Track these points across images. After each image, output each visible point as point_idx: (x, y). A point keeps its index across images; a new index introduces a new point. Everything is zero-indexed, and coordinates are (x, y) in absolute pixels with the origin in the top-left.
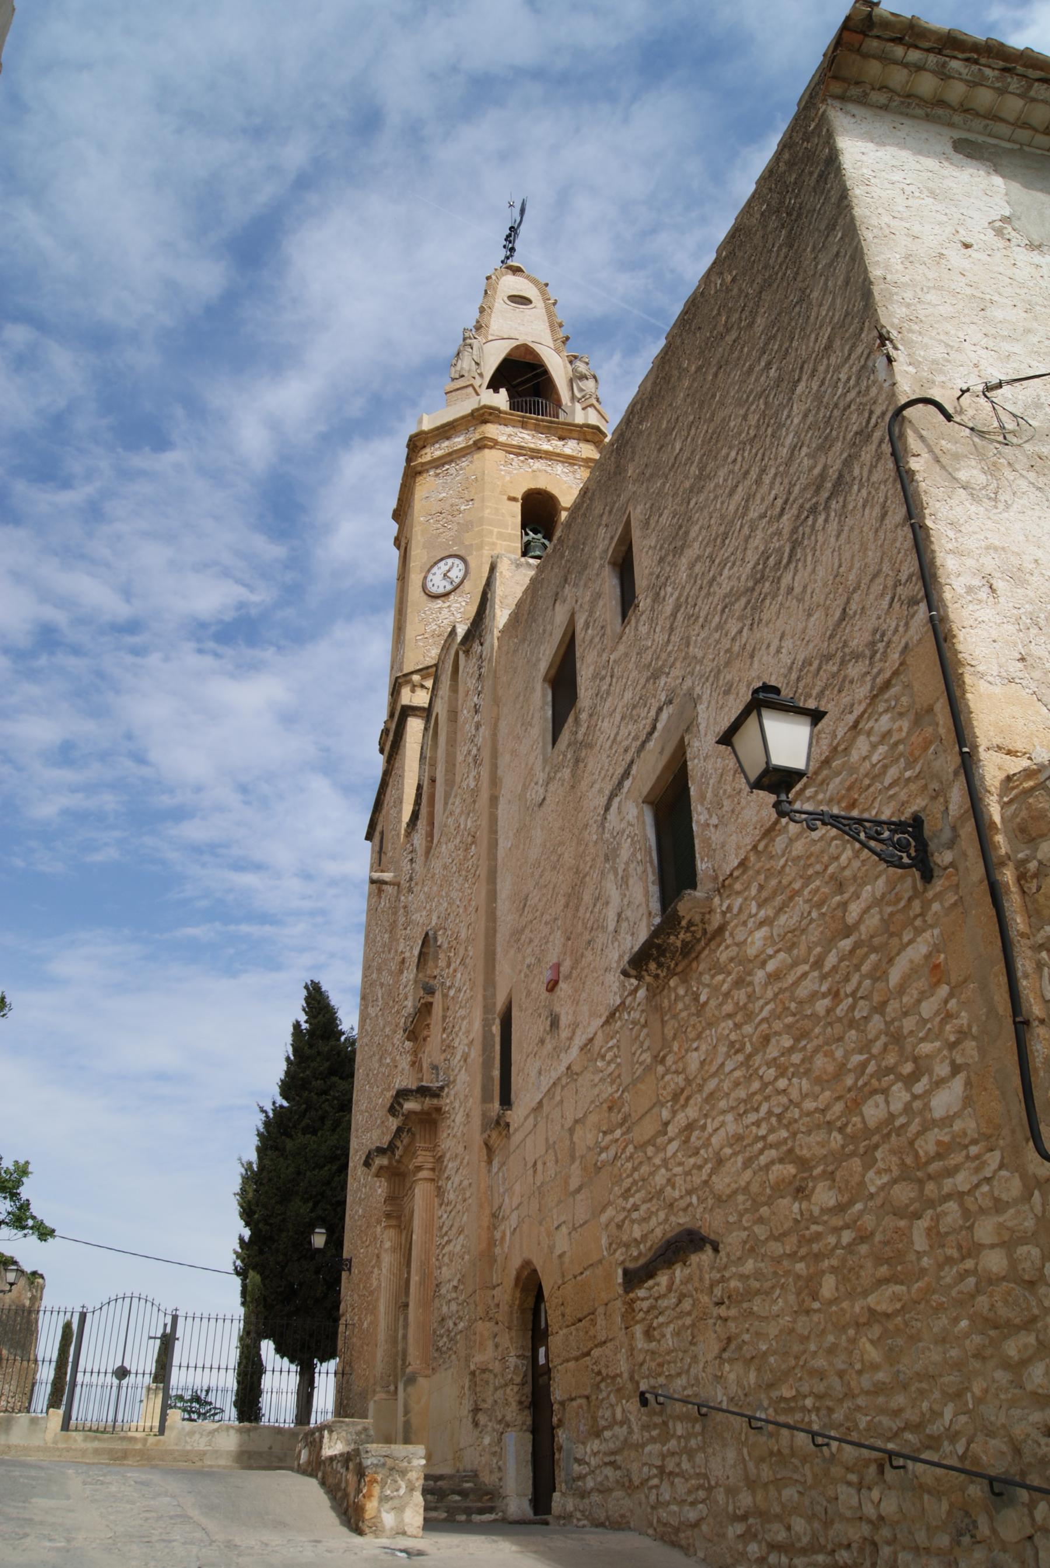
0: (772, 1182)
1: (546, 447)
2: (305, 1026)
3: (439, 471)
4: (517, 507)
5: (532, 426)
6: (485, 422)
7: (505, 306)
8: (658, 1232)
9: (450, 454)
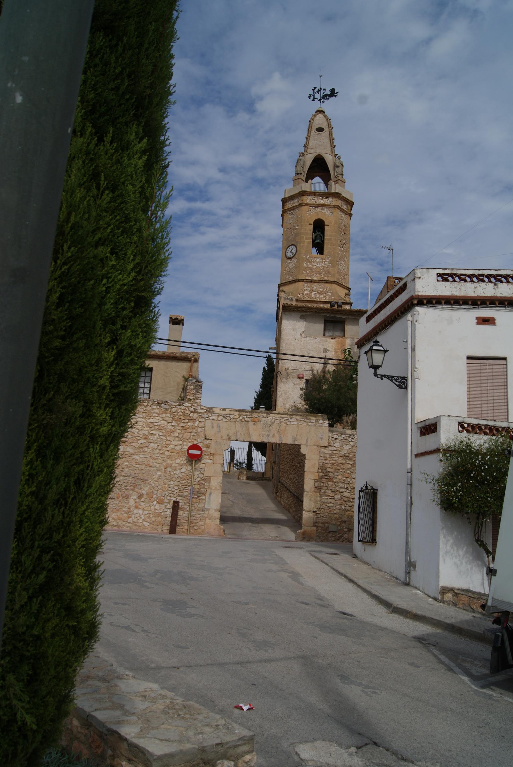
1: (322, 202)
2: (266, 368)
4: (311, 227)
6: (303, 195)
7: (315, 133)
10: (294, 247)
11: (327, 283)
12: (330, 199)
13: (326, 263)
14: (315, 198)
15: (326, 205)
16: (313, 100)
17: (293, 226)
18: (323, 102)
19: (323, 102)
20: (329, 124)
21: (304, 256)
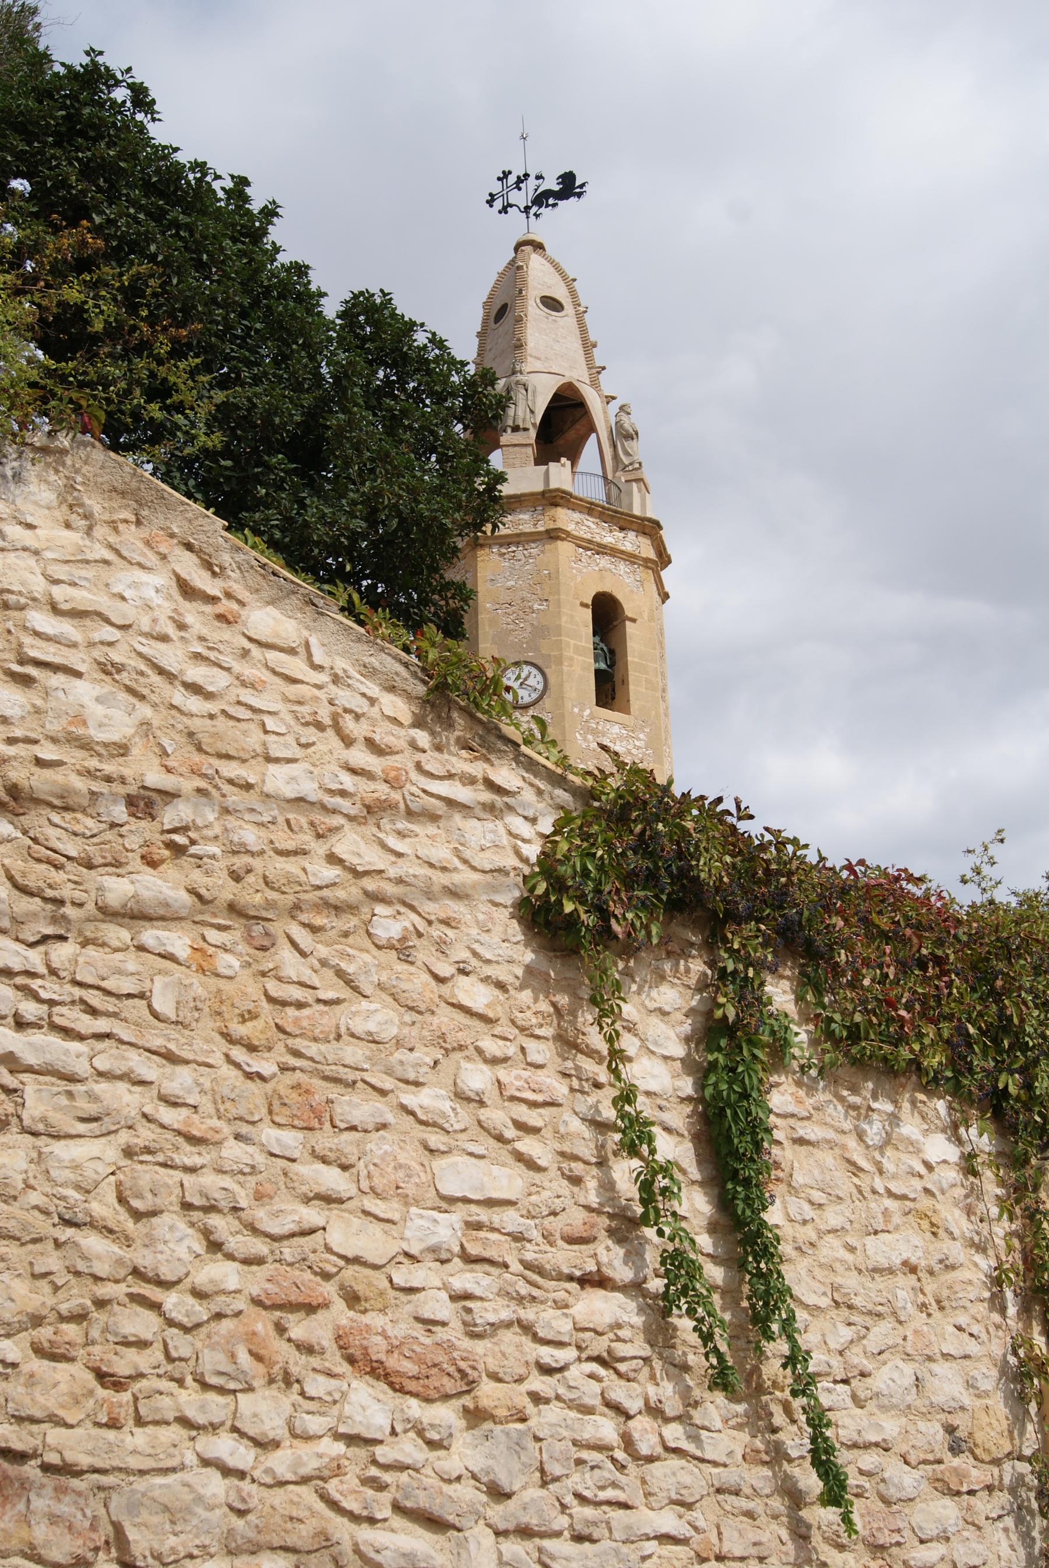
3: (504, 551)
4: (588, 614)
6: (556, 505)
7: (538, 311)
8: (335, 1090)
9: (518, 535)
10: (534, 671)
12: (631, 535)
13: (637, 743)
14: (590, 522)
15: (622, 552)
16: (504, 210)
17: (523, 600)
18: (537, 216)
19: (537, 216)
20: (573, 294)
21: (576, 710)
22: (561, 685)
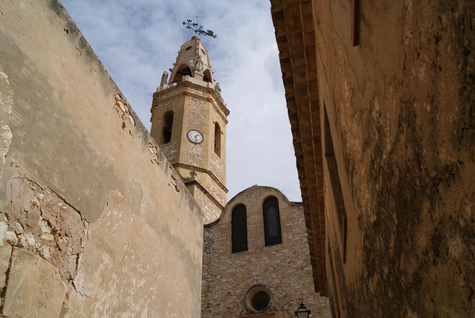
0: (443, 166)
3: (193, 98)
5: (217, 102)
6: (210, 93)
11: (223, 188)
17: (198, 114)
22: (208, 141)
